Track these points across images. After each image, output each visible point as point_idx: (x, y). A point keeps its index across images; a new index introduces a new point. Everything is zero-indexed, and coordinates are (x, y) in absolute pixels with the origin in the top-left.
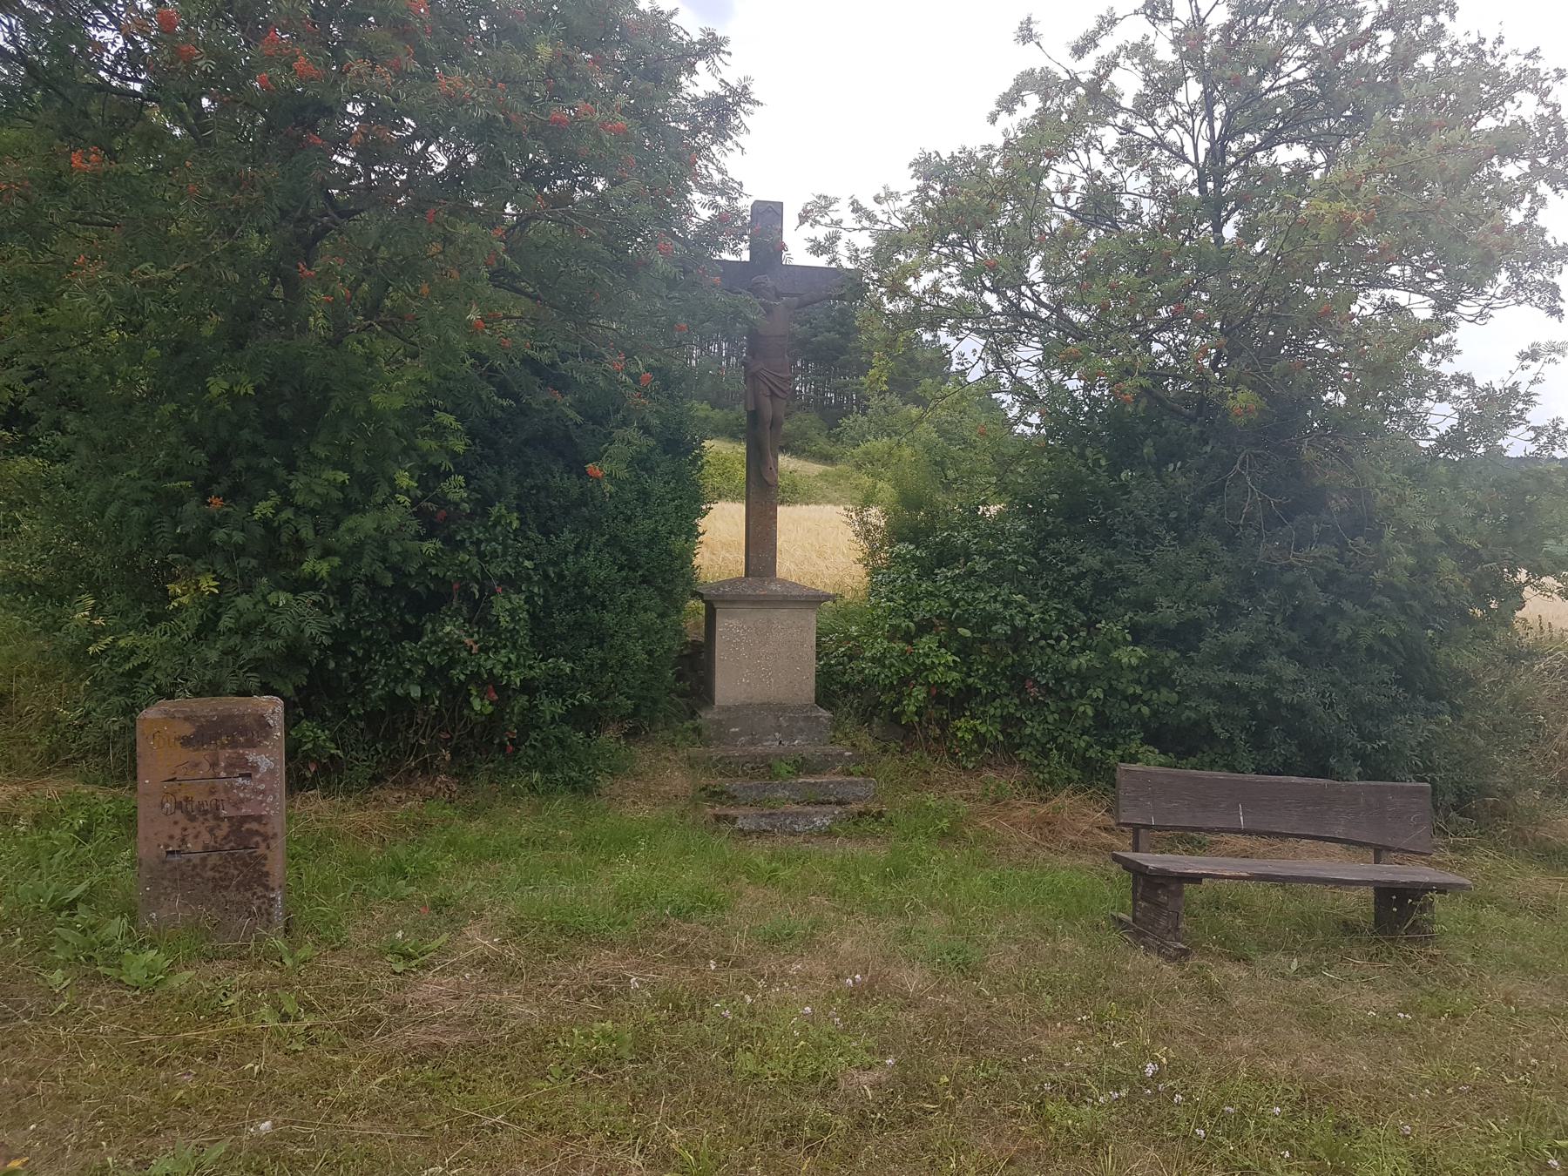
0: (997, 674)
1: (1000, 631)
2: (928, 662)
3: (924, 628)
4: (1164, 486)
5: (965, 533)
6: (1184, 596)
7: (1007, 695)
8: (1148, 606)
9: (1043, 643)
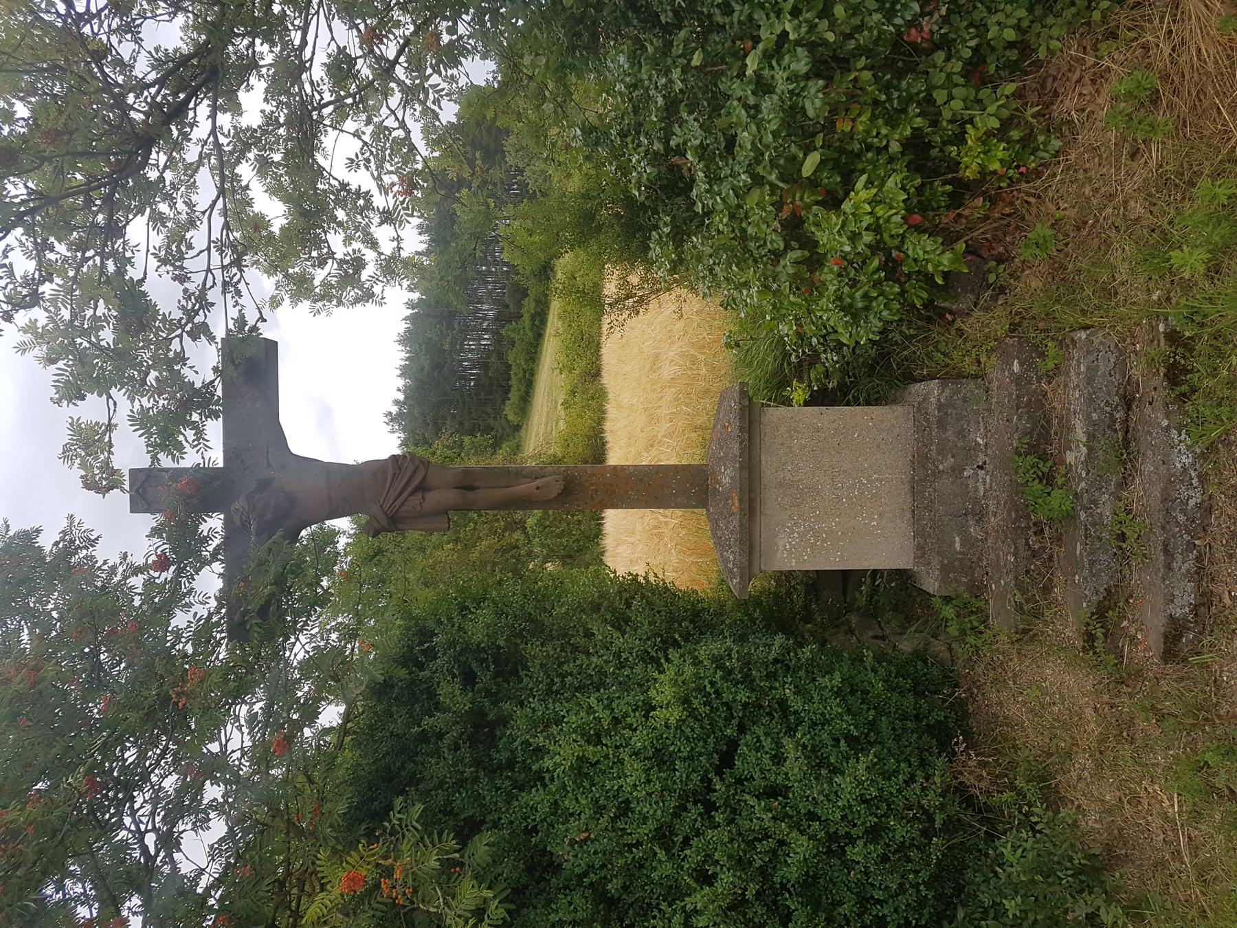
1: (818, 103)
2: (868, 238)
3: (794, 229)
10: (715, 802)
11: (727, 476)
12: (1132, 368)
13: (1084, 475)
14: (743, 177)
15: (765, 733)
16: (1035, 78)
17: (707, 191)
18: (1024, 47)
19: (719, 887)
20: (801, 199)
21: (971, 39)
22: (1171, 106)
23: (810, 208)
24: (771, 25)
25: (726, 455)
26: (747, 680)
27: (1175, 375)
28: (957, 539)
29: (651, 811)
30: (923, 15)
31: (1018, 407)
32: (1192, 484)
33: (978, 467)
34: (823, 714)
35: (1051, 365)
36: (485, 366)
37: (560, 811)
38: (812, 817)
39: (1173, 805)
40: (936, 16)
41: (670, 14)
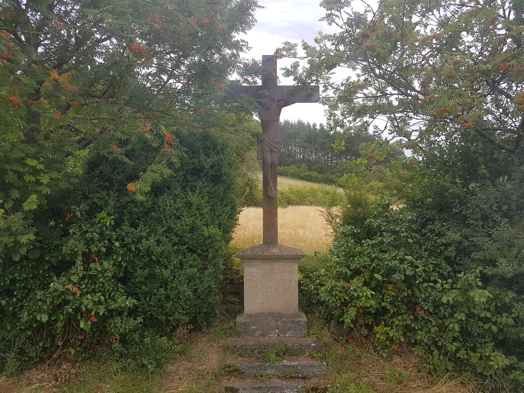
0: (399, 301)
2: (355, 294)
3: (357, 273)
4: (498, 190)
6: (516, 257)
7: (406, 313)
8: (493, 263)
9: (425, 285)
11: (275, 251)
14: (374, 255)
17: (369, 244)
18: (415, 344)
20: (367, 275)
21: (418, 327)
22: (398, 387)
24: (421, 264)
25: (282, 251)
26: (214, 257)
28: (255, 328)
29: (177, 226)
30: (425, 311)
31: (300, 345)
36: (289, 156)
40: (424, 315)
41: (425, 232)
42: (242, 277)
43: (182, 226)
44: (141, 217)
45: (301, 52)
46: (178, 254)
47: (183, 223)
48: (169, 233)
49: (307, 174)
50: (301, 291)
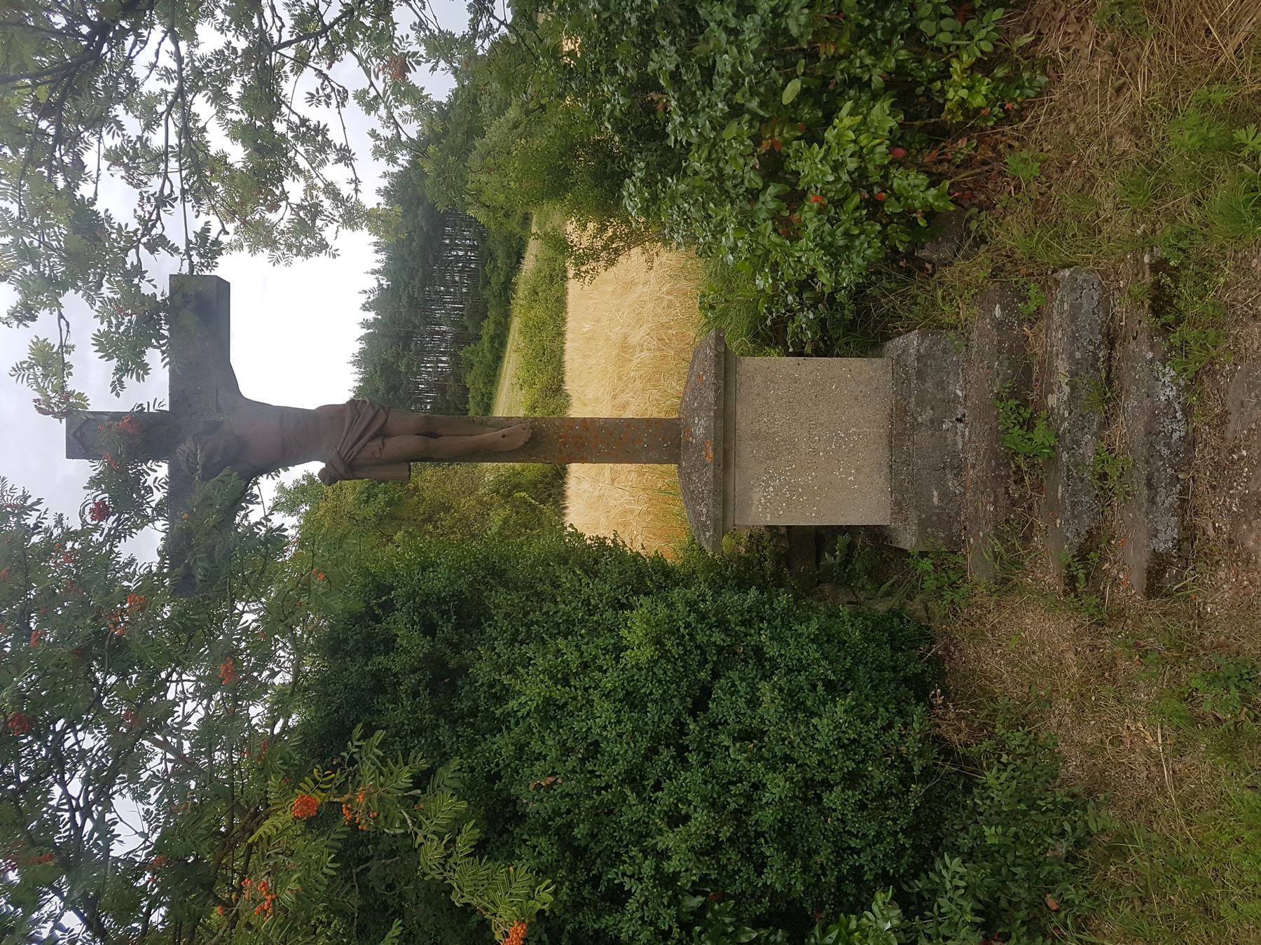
3: (773, 167)
5: (607, 88)
10: (687, 746)
11: (701, 427)
12: (1115, 306)
13: (1066, 415)
15: (740, 678)
16: (1019, 21)
19: (693, 826)
20: (781, 134)
23: (790, 144)
25: (700, 405)
26: (722, 624)
27: (1161, 301)
28: (935, 493)
32: (1176, 417)
33: (957, 419)
34: (799, 660)
35: (1033, 308)
36: (442, 389)
37: (525, 757)
38: (787, 758)
39: (1157, 740)
42: (770, 528)
43: (620, 735)
44: (589, 871)
45: (45, 326)
46: (713, 745)
47: (611, 734)
48: (643, 778)
49: (486, 345)
50: (824, 349)
